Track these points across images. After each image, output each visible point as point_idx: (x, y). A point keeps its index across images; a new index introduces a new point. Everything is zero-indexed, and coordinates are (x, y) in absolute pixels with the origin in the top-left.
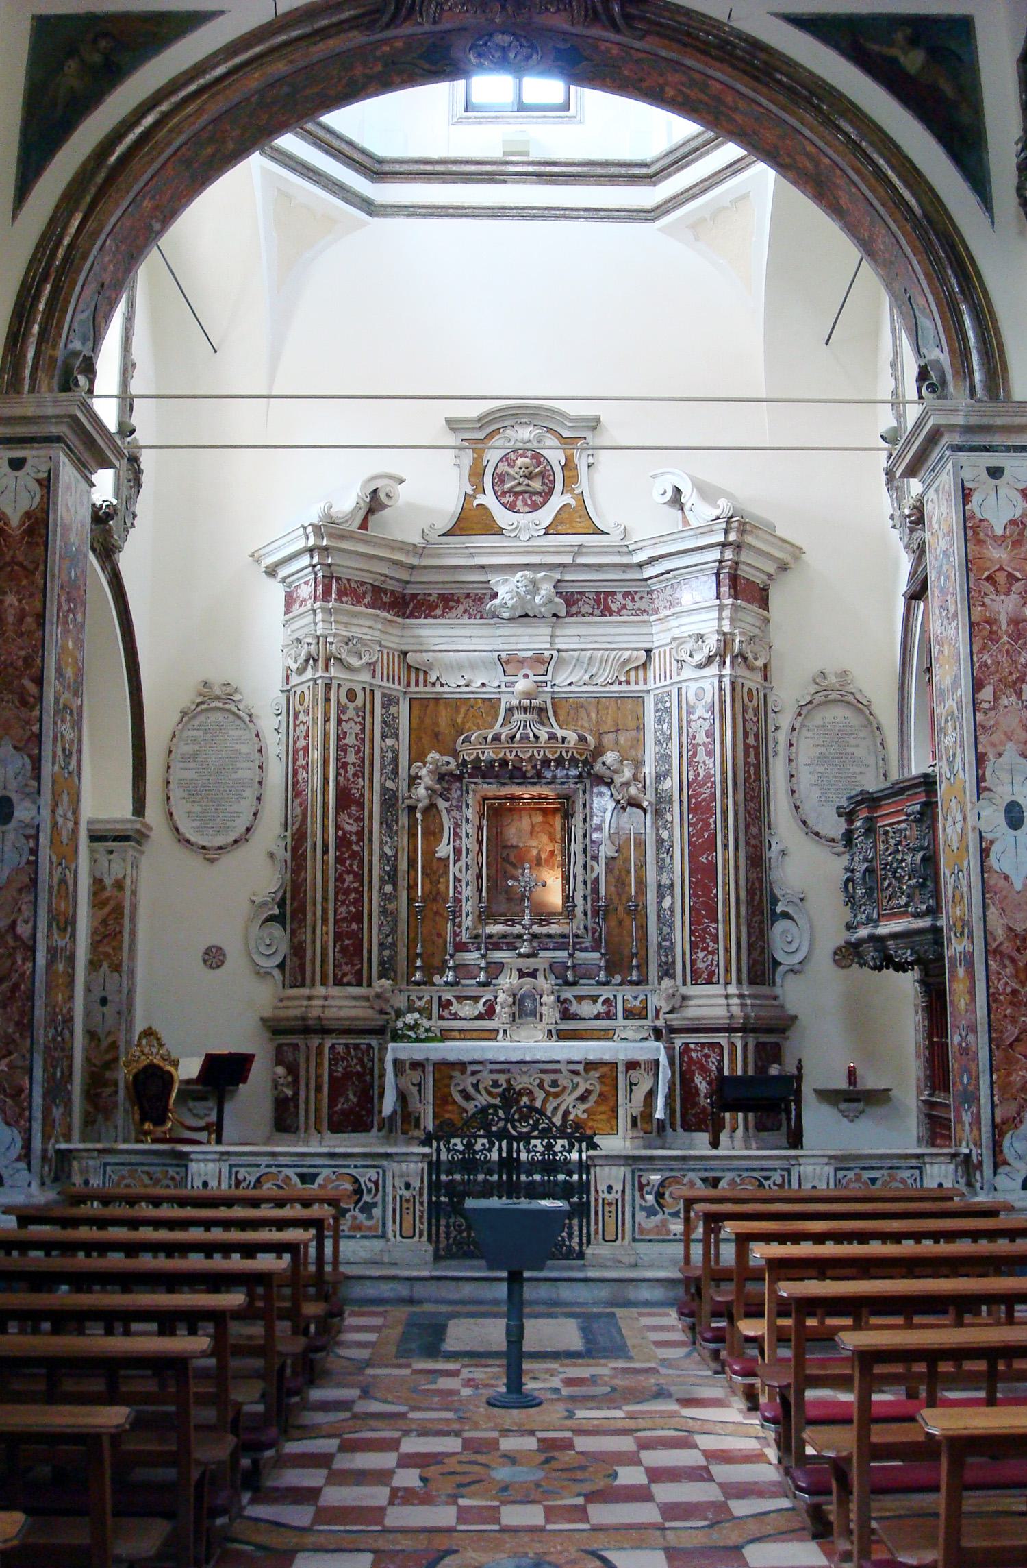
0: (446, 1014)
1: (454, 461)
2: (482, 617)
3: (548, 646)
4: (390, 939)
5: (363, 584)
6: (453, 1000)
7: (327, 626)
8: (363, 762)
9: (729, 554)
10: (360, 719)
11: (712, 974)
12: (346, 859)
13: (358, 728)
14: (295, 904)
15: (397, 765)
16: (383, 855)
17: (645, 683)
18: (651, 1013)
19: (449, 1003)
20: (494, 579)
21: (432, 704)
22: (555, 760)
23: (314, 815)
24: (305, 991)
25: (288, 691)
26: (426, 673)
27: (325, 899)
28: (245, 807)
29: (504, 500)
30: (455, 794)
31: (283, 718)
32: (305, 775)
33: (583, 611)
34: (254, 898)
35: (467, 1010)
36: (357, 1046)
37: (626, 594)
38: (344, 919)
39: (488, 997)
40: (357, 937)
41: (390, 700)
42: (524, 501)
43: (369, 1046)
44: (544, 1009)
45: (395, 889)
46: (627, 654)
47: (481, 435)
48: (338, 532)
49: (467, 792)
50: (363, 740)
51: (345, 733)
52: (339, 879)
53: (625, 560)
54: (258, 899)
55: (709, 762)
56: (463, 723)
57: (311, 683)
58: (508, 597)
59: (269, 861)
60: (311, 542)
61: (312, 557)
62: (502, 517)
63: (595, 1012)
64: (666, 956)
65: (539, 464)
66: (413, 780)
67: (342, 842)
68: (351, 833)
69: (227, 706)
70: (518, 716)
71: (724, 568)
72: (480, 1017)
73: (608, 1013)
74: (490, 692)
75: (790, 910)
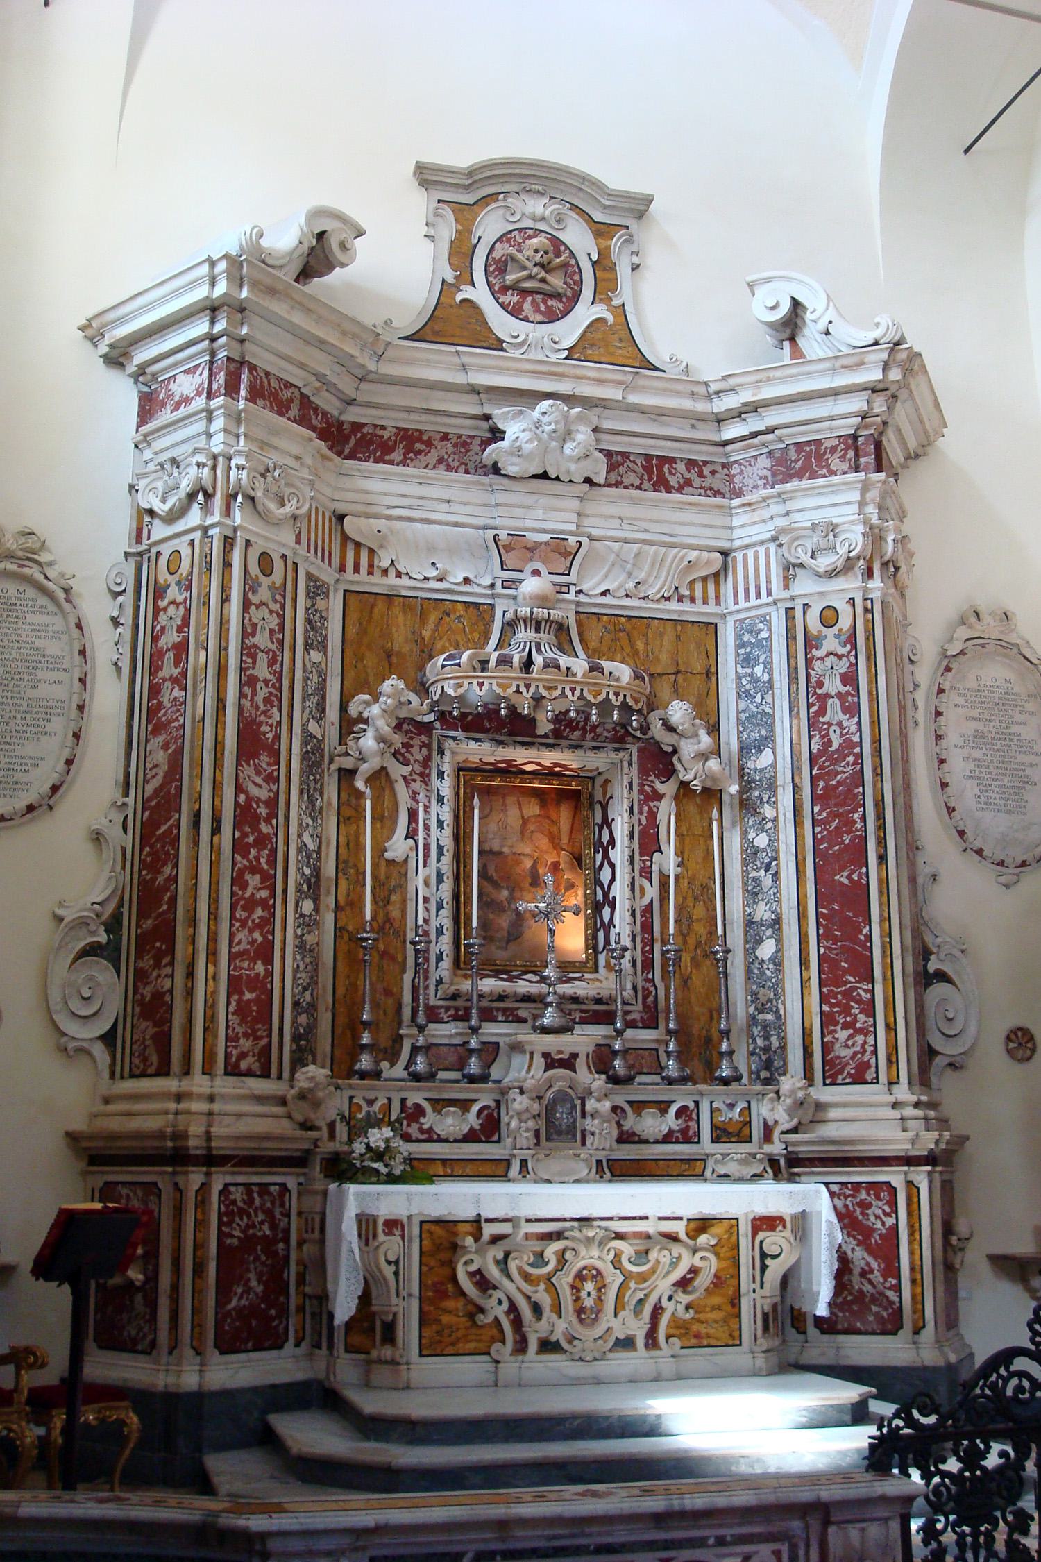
0: (413, 1130)
1: (425, 230)
2: (467, 472)
3: (573, 527)
4: (307, 995)
5: (289, 385)
6: (426, 1105)
7: (232, 441)
8: (280, 679)
9: (880, 405)
10: (276, 607)
11: (863, 1067)
12: (248, 846)
13: (273, 622)
14: (148, 924)
15: (324, 698)
16: (302, 847)
17: (718, 603)
18: (757, 1132)
19: (419, 1111)
20: (501, 414)
21: (381, 606)
22: (598, 705)
23: (198, 764)
24: (170, 1084)
25: (140, 554)
26: (371, 552)
27: (213, 915)
28: (52, 749)
29: (506, 299)
30: (418, 754)
31: (127, 599)
32: (177, 692)
33: (626, 481)
34: (61, 912)
35: (450, 1123)
36: (264, 1188)
37: (691, 463)
38: (241, 954)
39: (486, 1100)
40: (262, 986)
41: (317, 589)
42: (534, 303)
43: (283, 1187)
44: (590, 1125)
45: (317, 909)
46: (693, 555)
47: (469, 199)
48: (268, 281)
49: (442, 753)
50: (281, 643)
51: (254, 626)
52: (238, 881)
53: (701, 407)
54: (69, 915)
55: (851, 724)
56: (433, 638)
57: (197, 535)
58: (525, 436)
59: (89, 847)
60: (221, 288)
61: (213, 322)
62: (500, 322)
63: (665, 1130)
64: (766, 1037)
65: (558, 255)
66: (350, 725)
67: (245, 815)
68: (259, 800)
69: (26, 571)
70: (524, 635)
71: (867, 427)
72: (470, 1137)
73: (684, 1131)
74: (475, 595)
75: (947, 968)
